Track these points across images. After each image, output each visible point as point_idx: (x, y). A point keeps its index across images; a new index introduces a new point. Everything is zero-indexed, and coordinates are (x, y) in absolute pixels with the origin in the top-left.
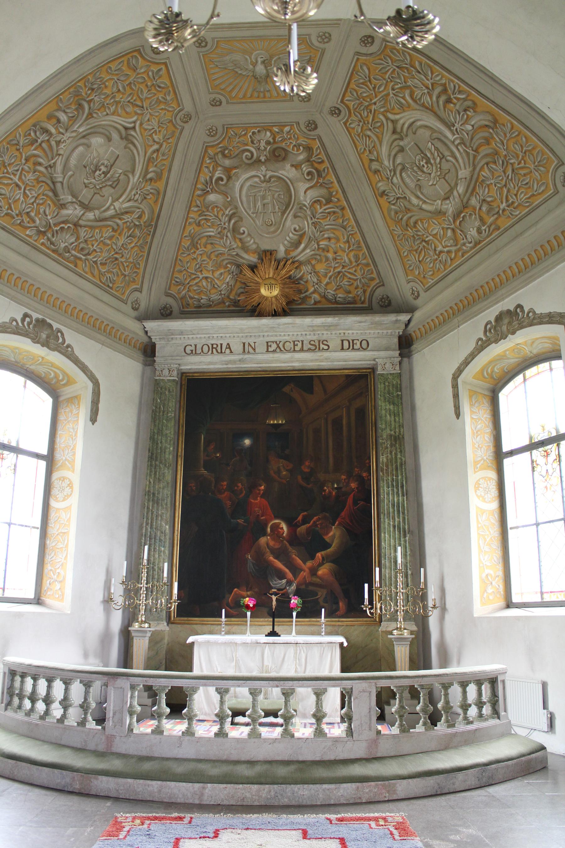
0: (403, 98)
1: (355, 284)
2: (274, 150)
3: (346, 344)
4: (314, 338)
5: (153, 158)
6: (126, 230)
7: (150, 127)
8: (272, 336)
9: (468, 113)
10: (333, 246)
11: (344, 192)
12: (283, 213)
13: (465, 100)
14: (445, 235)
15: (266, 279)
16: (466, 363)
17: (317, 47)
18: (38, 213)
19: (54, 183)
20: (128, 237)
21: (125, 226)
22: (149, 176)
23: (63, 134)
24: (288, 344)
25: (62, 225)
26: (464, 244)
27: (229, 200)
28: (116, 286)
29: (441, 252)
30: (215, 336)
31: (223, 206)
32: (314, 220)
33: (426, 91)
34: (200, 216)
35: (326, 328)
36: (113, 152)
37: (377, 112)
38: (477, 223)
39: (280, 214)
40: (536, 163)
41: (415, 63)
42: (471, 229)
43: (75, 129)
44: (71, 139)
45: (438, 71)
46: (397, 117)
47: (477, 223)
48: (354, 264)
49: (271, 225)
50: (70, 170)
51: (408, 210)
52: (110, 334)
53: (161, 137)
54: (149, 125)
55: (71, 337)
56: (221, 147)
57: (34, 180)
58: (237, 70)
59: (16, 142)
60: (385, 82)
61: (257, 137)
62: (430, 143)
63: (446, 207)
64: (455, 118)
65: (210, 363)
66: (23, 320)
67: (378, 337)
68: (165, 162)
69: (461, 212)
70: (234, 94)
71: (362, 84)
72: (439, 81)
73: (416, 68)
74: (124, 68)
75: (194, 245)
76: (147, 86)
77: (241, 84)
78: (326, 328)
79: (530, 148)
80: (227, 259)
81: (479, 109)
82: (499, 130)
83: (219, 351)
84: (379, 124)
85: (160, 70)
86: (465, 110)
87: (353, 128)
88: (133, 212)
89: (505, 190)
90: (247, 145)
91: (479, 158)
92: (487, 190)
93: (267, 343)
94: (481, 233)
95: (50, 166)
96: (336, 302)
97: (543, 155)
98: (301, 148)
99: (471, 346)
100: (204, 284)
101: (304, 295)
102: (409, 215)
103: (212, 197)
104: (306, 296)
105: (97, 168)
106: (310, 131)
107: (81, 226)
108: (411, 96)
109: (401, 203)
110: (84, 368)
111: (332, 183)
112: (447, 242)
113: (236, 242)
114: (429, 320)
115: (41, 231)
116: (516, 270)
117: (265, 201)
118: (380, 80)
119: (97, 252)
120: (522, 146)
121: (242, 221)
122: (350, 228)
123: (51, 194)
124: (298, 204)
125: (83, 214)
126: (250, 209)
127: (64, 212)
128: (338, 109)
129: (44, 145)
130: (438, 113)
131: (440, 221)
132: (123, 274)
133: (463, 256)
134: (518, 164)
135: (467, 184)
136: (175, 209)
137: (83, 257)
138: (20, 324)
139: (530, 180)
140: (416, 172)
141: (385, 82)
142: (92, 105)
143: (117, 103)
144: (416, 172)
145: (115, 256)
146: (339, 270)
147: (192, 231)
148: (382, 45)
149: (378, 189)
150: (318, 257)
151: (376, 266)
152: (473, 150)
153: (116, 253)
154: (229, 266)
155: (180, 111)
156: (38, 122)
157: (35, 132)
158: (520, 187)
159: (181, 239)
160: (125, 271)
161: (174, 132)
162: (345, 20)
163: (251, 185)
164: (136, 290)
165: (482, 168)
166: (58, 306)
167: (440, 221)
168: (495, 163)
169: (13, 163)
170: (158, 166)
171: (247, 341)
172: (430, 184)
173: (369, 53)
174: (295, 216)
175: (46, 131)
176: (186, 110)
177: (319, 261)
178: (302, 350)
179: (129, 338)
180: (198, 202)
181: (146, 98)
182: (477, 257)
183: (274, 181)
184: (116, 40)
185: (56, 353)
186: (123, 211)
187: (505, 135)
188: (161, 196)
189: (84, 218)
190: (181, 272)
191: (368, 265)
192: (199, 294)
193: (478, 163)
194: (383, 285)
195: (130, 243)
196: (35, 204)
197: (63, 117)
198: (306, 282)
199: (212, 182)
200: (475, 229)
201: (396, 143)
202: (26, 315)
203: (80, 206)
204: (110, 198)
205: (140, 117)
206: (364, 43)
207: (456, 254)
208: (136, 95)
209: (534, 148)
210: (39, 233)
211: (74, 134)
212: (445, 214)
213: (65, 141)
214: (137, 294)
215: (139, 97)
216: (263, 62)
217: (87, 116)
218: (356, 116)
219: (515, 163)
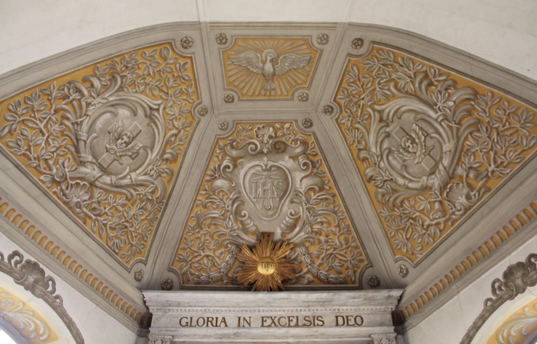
0: (389, 90)
1: (346, 266)
2: (275, 144)
3: (340, 320)
4: (310, 314)
5: (171, 141)
6: (138, 202)
7: (172, 113)
8: (267, 311)
9: (449, 91)
10: (325, 230)
11: (335, 180)
12: (281, 198)
13: (445, 80)
14: (432, 208)
15: (263, 258)
16: (476, 327)
17: (316, 48)
18: (56, 163)
19: (77, 140)
20: (139, 209)
21: (138, 197)
22: (166, 156)
23: (94, 98)
24: (282, 319)
25: (78, 181)
26: (453, 213)
27: (233, 185)
28: (122, 252)
29: (429, 226)
30: (211, 309)
31: (228, 190)
32: (308, 206)
33: (409, 80)
34: (207, 198)
35: (321, 303)
36: (136, 127)
37: (365, 106)
38: (465, 191)
39: (278, 199)
40: (522, 122)
41: (398, 59)
42: (460, 198)
43: (106, 96)
44: (100, 105)
45: (418, 61)
46: (383, 107)
47: (465, 191)
48: (344, 246)
49: (270, 209)
50: (94, 131)
51: (395, 191)
52: (108, 297)
53: (180, 124)
54: (171, 111)
55: (63, 288)
56: (230, 140)
57: (60, 131)
58: (249, 67)
59: (49, 93)
60: (372, 79)
61: (261, 132)
62: (414, 125)
63: (432, 181)
64: (437, 98)
65: (205, 336)
66: (11, 257)
67: (371, 314)
68: (181, 147)
69: (447, 183)
70: (245, 91)
71: (353, 82)
72: (420, 69)
73: (398, 63)
74: (156, 56)
75: (199, 225)
76: (173, 76)
77: (252, 81)
78: (321, 303)
79: (513, 110)
80: (228, 239)
81: (459, 86)
82: (480, 101)
83: (214, 324)
84: (367, 116)
85: (186, 63)
86: (446, 89)
87: (344, 124)
88: (147, 186)
89: (492, 154)
90: (252, 138)
91: (462, 129)
92: (472, 158)
93: (263, 318)
94: (470, 199)
95: (77, 124)
96: (329, 282)
97: (528, 112)
98: (299, 142)
99: (479, 308)
100: (205, 261)
101: (297, 275)
102: (396, 195)
103: (219, 183)
104: (300, 276)
105: (120, 137)
106: (306, 128)
107: (96, 187)
108: (396, 87)
109: (388, 185)
110: (70, 324)
111: (324, 173)
112: (434, 215)
113: (237, 224)
114: (422, 293)
115: (56, 181)
116: (519, 223)
117: (266, 188)
118: (367, 78)
119: (108, 215)
120: (505, 111)
121: (244, 205)
122: (340, 214)
123: (73, 149)
124: (295, 191)
125: (100, 177)
126: (252, 194)
127: (83, 169)
128: (331, 107)
129: (75, 103)
130: (421, 96)
131: (426, 196)
132: (130, 243)
133: (453, 224)
134: (503, 126)
135: (452, 155)
136: (186, 191)
137: (94, 217)
138: (6, 260)
139: (518, 138)
140: (402, 154)
141: (372, 79)
142: (124, 80)
143: (147, 84)
144: (402, 154)
145: (125, 224)
146: (331, 251)
147: (199, 212)
148: (369, 47)
149: (366, 176)
150: (312, 240)
151: (364, 248)
152: (456, 124)
153: (127, 221)
154: (229, 245)
155: (199, 104)
156: (73, 81)
157: (69, 89)
158: (508, 147)
159: (188, 219)
160: (133, 240)
161: (191, 122)
162: (341, 23)
163: (254, 173)
164: (141, 261)
165: (466, 139)
166: (57, 256)
167: (426, 196)
168: (478, 131)
169: (42, 111)
170: (175, 149)
171: (242, 315)
172: (416, 162)
173: (359, 54)
174: (292, 202)
175: (79, 91)
176: (203, 104)
177: (313, 244)
178: (297, 325)
179: (127, 306)
180: (206, 186)
181: (172, 87)
182: (469, 222)
183: (274, 170)
184: (153, 29)
185: (41, 300)
186: (138, 183)
187: (487, 103)
188: (174, 178)
189: (100, 180)
190: (185, 249)
191: (356, 247)
192: (199, 271)
193: (462, 135)
194: (372, 266)
195: (140, 215)
196: (55, 154)
197: (97, 83)
198: (301, 263)
199: (220, 169)
200: (464, 196)
201: (382, 131)
202: (16, 253)
203: (99, 168)
204: (128, 168)
205: (164, 102)
206: (355, 45)
207: (445, 225)
208: (163, 82)
209: (517, 109)
210: (54, 181)
211: (104, 101)
212: (431, 188)
213: (94, 105)
214: (141, 266)
215: (166, 84)
216: (272, 61)
217: (119, 89)
218: (346, 112)
219: (499, 126)
